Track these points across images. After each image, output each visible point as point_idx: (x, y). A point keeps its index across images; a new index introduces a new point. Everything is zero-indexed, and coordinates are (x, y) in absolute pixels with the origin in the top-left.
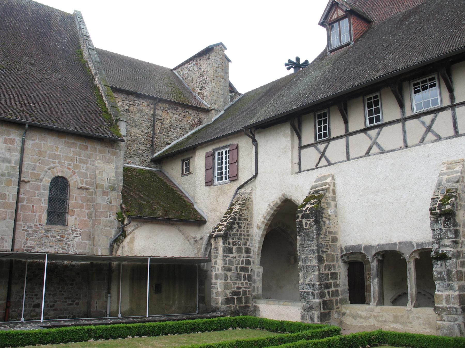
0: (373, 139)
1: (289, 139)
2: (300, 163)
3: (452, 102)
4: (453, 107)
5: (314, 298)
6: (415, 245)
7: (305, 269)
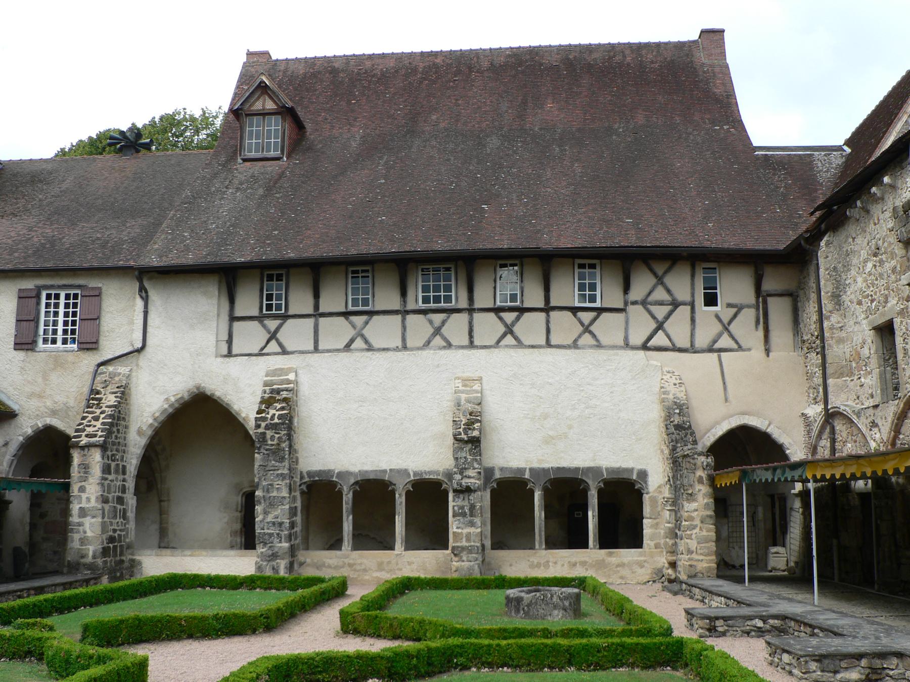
0: (358, 328)
1: (215, 301)
2: (230, 342)
3: (470, 305)
4: (471, 310)
5: (280, 542)
6: (412, 474)
7: (268, 502)
